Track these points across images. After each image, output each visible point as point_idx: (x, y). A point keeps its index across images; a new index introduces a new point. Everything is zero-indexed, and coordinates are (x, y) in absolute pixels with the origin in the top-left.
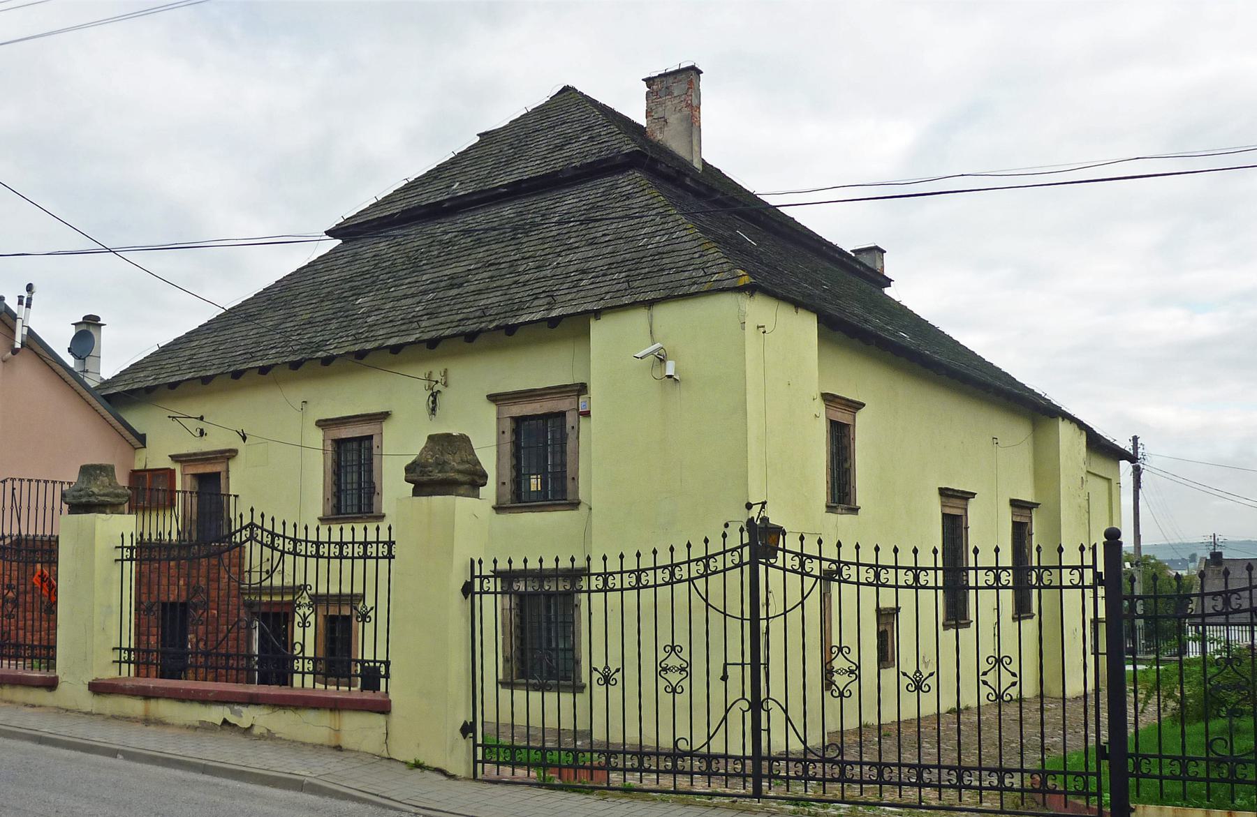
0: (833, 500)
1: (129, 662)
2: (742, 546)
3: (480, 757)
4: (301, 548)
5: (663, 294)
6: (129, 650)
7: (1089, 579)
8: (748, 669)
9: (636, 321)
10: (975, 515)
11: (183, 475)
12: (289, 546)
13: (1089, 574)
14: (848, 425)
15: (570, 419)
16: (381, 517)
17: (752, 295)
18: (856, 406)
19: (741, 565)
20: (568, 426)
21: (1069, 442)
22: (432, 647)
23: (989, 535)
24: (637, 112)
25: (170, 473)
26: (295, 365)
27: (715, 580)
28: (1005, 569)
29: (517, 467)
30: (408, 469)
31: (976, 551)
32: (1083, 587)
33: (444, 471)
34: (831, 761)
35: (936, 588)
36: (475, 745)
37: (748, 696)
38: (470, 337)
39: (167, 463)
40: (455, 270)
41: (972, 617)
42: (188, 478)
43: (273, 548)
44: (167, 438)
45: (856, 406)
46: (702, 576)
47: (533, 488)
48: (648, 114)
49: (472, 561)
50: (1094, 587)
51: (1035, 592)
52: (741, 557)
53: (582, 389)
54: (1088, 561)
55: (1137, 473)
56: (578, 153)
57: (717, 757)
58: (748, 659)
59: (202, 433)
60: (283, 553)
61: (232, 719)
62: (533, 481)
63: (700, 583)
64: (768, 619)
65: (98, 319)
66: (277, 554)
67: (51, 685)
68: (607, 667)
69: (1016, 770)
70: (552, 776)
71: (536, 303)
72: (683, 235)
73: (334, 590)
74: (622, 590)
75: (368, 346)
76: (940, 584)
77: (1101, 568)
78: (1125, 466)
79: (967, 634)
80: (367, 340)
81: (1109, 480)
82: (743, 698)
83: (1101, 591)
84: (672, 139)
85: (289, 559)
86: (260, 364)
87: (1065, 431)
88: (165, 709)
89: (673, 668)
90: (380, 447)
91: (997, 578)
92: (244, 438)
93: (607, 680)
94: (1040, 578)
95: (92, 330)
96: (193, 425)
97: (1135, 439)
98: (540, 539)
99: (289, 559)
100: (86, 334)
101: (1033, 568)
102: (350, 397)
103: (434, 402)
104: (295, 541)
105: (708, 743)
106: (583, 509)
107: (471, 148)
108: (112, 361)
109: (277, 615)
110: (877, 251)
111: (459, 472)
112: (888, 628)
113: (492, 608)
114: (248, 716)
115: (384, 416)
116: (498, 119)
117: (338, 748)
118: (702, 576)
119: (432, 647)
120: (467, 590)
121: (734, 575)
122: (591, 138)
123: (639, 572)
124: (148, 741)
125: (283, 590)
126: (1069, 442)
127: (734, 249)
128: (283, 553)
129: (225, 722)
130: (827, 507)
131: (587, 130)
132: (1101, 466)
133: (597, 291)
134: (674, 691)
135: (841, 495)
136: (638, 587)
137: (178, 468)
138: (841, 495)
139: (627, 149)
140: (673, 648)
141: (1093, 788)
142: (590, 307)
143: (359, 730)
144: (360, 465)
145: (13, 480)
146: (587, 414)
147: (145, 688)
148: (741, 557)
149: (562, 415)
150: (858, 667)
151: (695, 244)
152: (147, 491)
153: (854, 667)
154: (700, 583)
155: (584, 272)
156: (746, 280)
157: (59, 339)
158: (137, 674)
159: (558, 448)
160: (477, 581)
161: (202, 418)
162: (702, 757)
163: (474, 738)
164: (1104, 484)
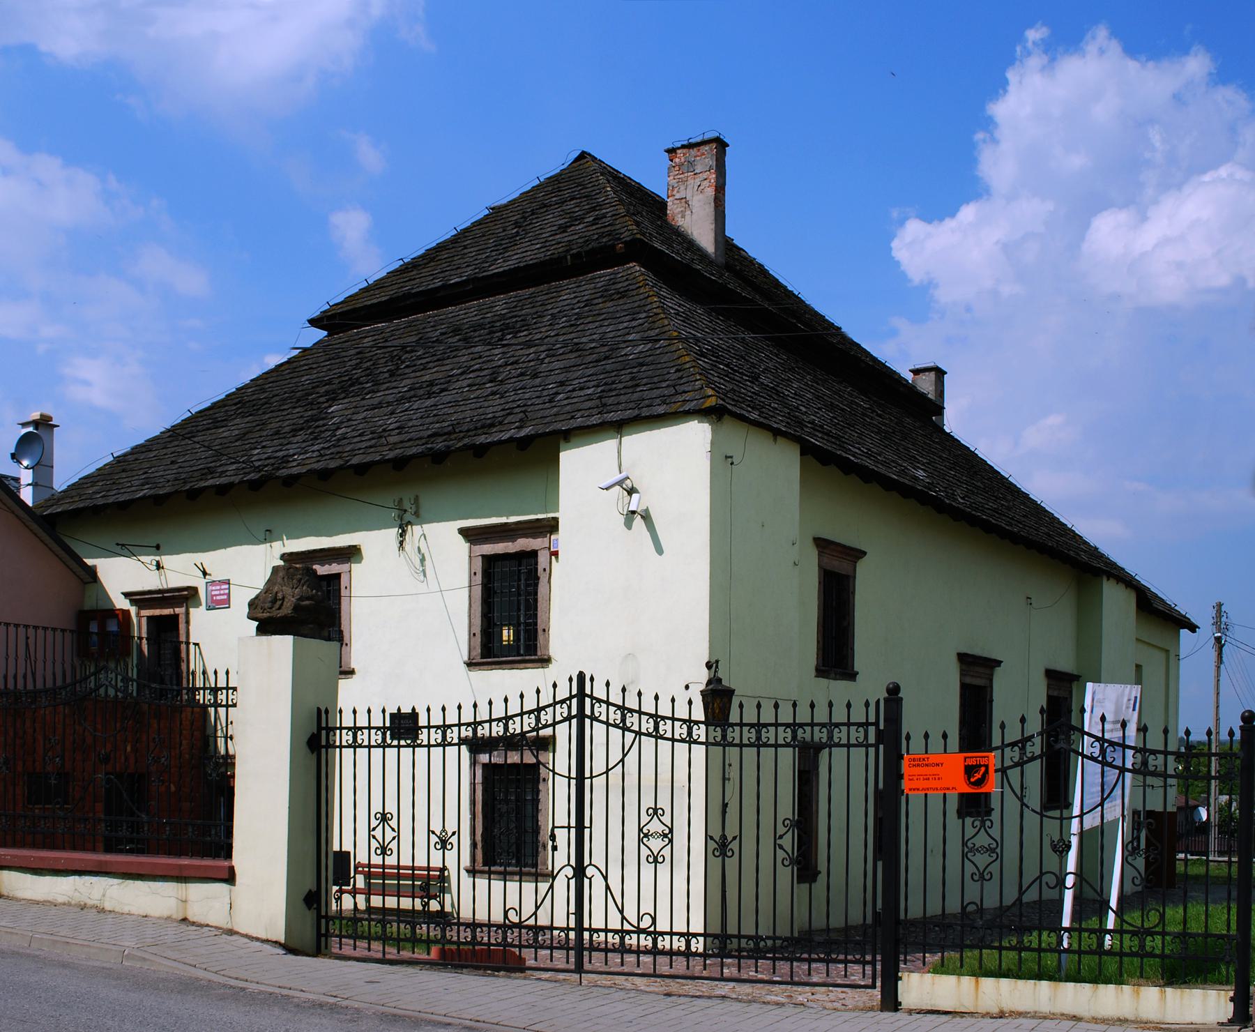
2: (571, 697)
4: (665, 727)
7: (872, 740)
8: (573, 831)
13: (872, 729)
14: (847, 577)
15: (543, 559)
18: (857, 554)
19: (569, 718)
21: (1115, 604)
26: (255, 486)
30: (252, 604)
32: (868, 746)
34: (644, 931)
36: (319, 917)
37: (573, 862)
38: (438, 458)
40: (435, 376)
45: (857, 554)
46: (1016, 765)
47: (505, 638)
49: (319, 710)
50: (876, 746)
51: (388, 724)
52: (570, 708)
53: (552, 526)
54: (872, 719)
57: (543, 928)
62: (505, 633)
64: (591, 777)
68: (444, 830)
69: (1086, 953)
70: (392, 952)
71: (510, 418)
75: (333, 464)
77: (882, 727)
81: (1167, 651)
82: (569, 865)
83: (881, 747)
86: (218, 481)
90: (349, 588)
105: (535, 913)
108: (74, 461)
117: (184, 920)
118: (1016, 765)
130: (817, 670)
131: (594, 209)
134: (656, 861)
142: (558, 426)
146: (556, 554)
148: (570, 708)
149: (534, 554)
150: (671, 831)
153: (1130, 859)
154: (1014, 774)
156: (711, 402)
160: (324, 733)
162: (529, 928)
164: (1163, 655)
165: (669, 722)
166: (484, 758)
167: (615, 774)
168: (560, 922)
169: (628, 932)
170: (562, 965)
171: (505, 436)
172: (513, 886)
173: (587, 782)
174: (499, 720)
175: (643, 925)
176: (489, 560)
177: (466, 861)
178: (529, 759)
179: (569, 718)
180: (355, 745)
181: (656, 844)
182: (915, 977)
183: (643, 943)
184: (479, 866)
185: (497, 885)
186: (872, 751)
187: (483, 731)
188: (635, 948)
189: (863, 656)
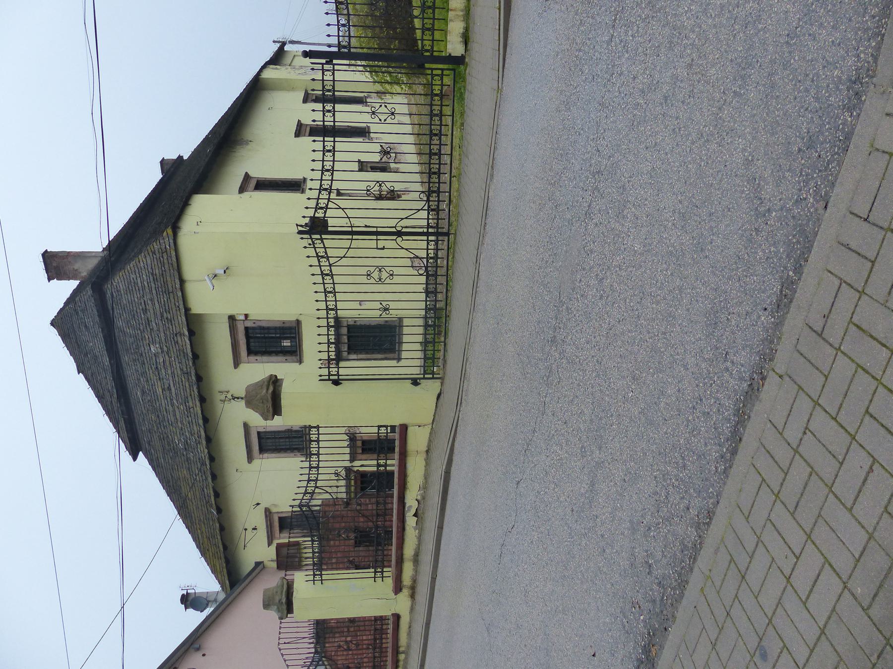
0: (298, 190)
1: (382, 572)
3: (431, 376)
5: (176, 274)
6: (375, 572)
8: (379, 237)
9: (190, 288)
10: (307, 121)
11: (280, 538)
12: (312, 484)
13: (326, 67)
14: (258, 181)
15: (249, 324)
16: (305, 180)
17: (179, 228)
18: (247, 177)
19: (322, 239)
20: (254, 325)
21: (270, 74)
22: (380, 398)
23: (312, 114)
24: (69, 286)
25: (279, 547)
26: (214, 477)
27: (330, 252)
28: (324, 107)
29: (277, 353)
31: (314, 121)
32: (334, 70)
33: (270, 397)
35: (334, 141)
36: (424, 378)
37: (395, 237)
38: (199, 379)
39: (273, 547)
41: (365, 125)
42: (282, 535)
43: (314, 492)
44: (257, 549)
45: (247, 177)
47: (289, 344)
48: (76, 279)
53: (232, 318)
55: (292, 42)
56: (92, 318)
58: (375, 237)
59: (255, 529)
60: (316, 487)
61: (413, 511)
62: (285, 344)
63: (332, 261)
65: (183, 595)
66: (317, 490)
67: (397, 617)
72: (142, 264)
73: (348, 450)
74: (336, 301)
76: (332, 139)
77: (324, 61)
78: (286, 48)
79: (373, 128)
80: (199, 437)
83: (335, 62)
84: (86, 268)
85: (319, 484)
86: (213, 498)
87: (266, 74)
88: (409, 551)
89: (380, 275)
91: (329, 111)
92: (258, 504)
93: (386, 309)
94: (329, 91)
95: (190, 598)
96: (250, 533)
97: (274, 42)
98: (315, 342)
99: (319, 484)
100: (189, 601)
101: (323, 94)
102: (233, 444)
103: (238, 398)
104: (309, 481)
106: (300, 319)
107: (86, 378)
108: (207, 582)
109: (362, 483)
110: (163, 162)
111: (268, 389)
112: (369, 165)
113: (352, 367)
114: (411, 501)
115: (246, 426)
116: (69, 363)
119: (380, 398)
120: (336, 383)
121: (327, 243)
122: (83, 311)
123: (326, 292)
124: (427, 558)
125: (347, 478)
126: (270, 74)
127: (157, 233)
128: (316, 487)
129: (415, 515)
131: (77, 313)
132: (287, 60)
133: (174, 310)
134: (392, 275)
135: (294, 186)
136: (334, 293)
137: (276, 542)
138: (294, 186)
139: (90, 292)
140: (368, 275)
141: (439, 72)
143: (417, 440)
144: (275, 438)
145: (279, 644)
146: (246, 316)
147: (397, 562)
149: (246, 329)
151: (148, 258)
152: (288, 560)
154: (332, 261)
155: (162, 316)
156: (170, 231)
157: (196, 618)
158: (390, 566)
159: (266, 331)
160: (331, 377)
161: (246, 529)
163: (420, 379)
165: (323, 182)
166: (345, 354)
167: (350, 213)
168: (424, 244)
169: (429, 207)
170: (446, 243)
171: (188, 342)
172: (405, 339)
173: (354, 229)
174: (323, 278)
175: (425, 199)
176: (250, 352)
177: (393, 363)
178: (344, 331)
179: (322, 239)
180: (324, 151)
181: (384, 275)
182: (449, 46)
183: (432, 247)
184: (396, 356)
185: (405, 347)
186: (336, 67)
187: (333, 355)
188: (435, 221)
189: (297, 175)
